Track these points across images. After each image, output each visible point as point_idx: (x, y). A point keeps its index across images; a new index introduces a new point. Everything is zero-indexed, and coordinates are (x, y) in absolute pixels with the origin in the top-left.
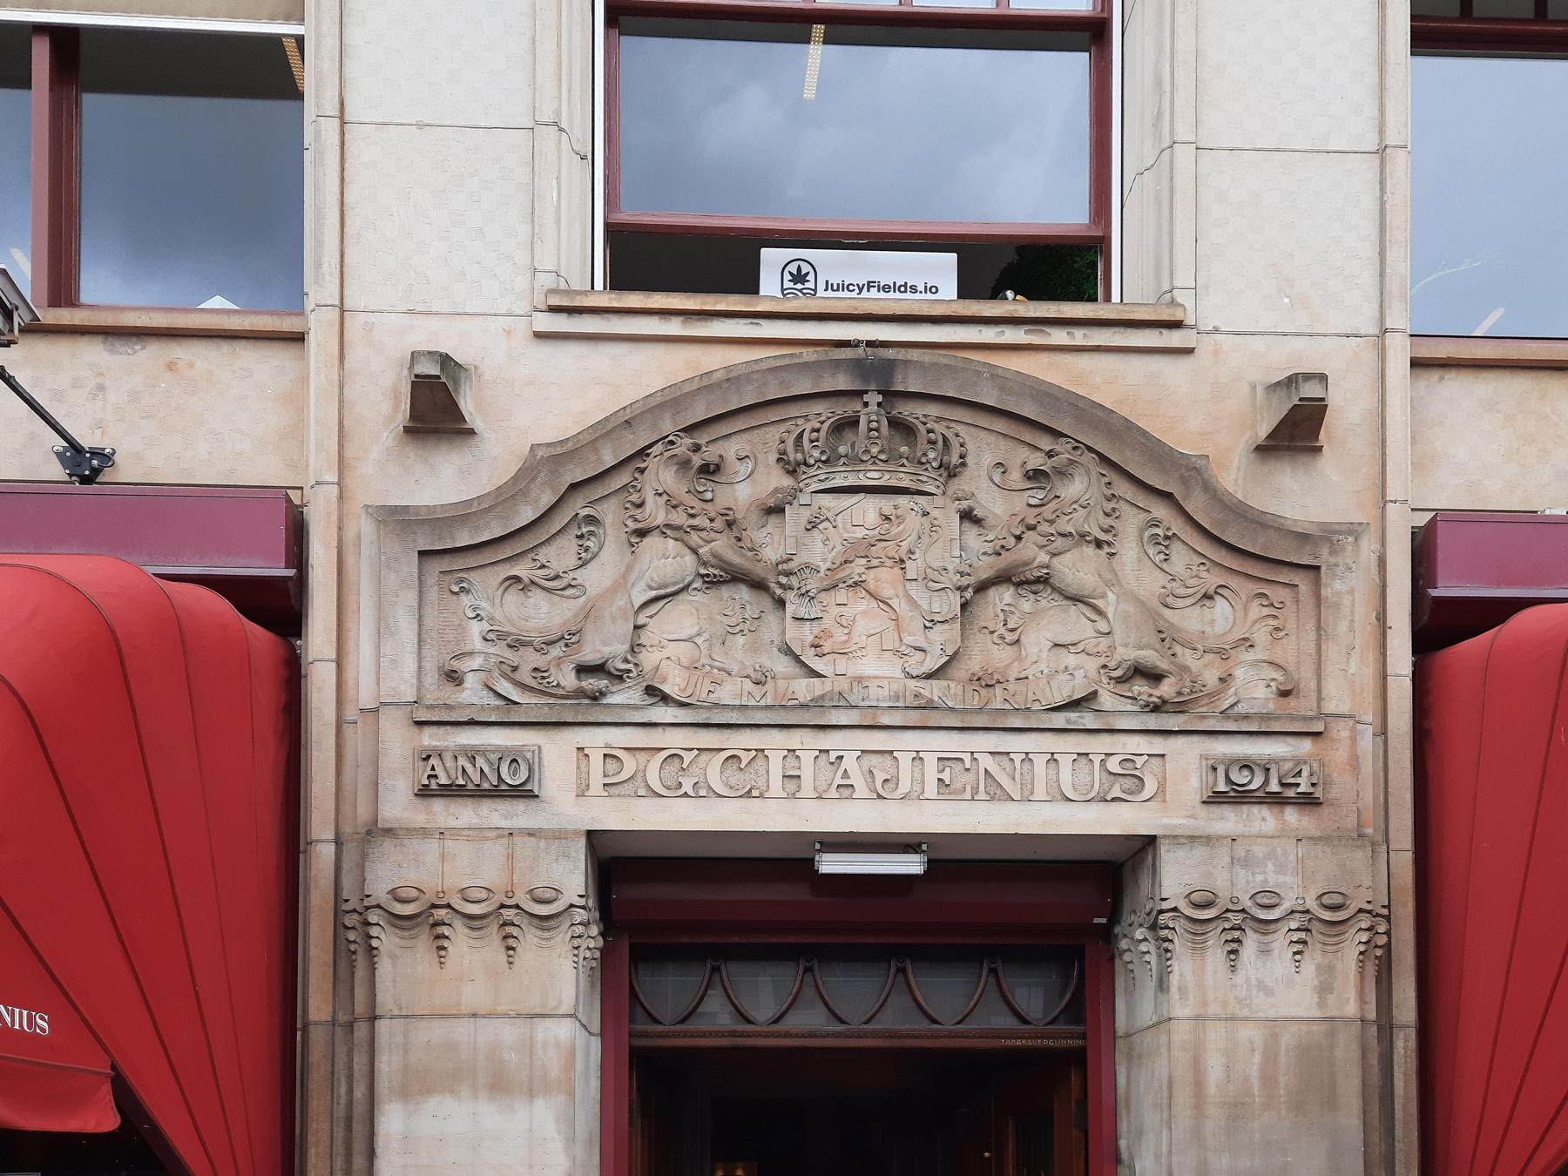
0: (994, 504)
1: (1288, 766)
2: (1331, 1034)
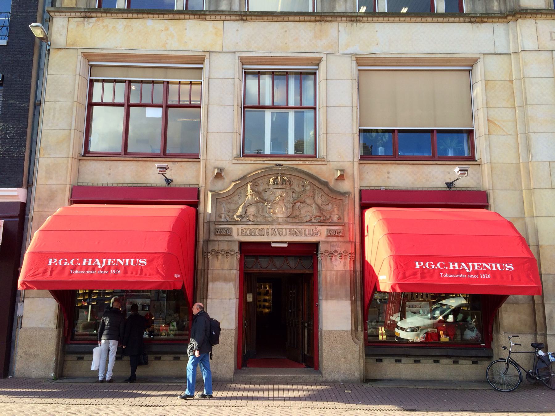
0: (297, 189)
1: (339, 231)
2: (346, 273)
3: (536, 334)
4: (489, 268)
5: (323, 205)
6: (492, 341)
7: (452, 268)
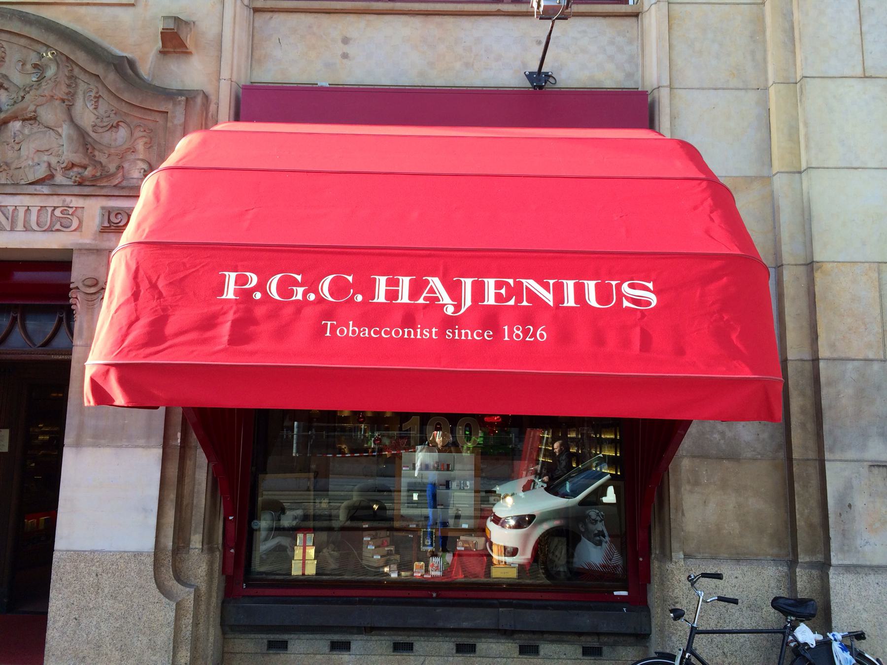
3: (793, 563)
4: (548, 297)
5: (100, 130)
6: (650, 582)
7: (381, 297)
